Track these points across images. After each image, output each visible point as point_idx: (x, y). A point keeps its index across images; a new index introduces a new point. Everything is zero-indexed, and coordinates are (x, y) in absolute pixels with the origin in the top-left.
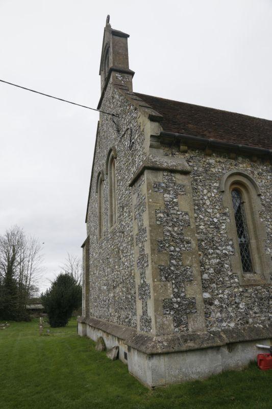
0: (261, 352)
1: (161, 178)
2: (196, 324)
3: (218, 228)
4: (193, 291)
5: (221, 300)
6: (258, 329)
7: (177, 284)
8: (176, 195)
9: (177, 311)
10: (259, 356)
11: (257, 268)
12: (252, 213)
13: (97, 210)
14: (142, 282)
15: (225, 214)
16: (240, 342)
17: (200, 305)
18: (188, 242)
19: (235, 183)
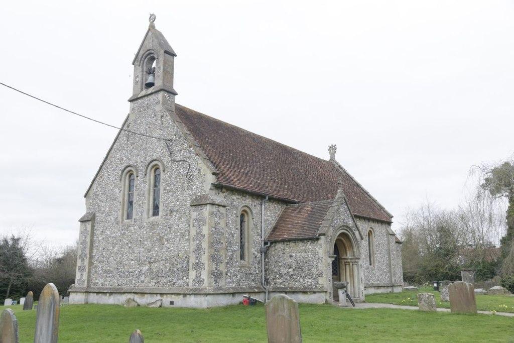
0: (244, 298)
1: (215, 209)
2: (222, 283)
3: (233, 236)
4: (222, 268)
5: (231, 273)
6: (244, 288)
7: (217, 264)
8: (220, 218)
9: (216, 276)
10: (401, 228)
11: (246, 259)
12: (248, 228)
13: (296, 285)
14: (197, 261)
15: (237, 229)
16: (237, 293)
17: (224, 274)
18: (222, 244)
19: (244, 211)
